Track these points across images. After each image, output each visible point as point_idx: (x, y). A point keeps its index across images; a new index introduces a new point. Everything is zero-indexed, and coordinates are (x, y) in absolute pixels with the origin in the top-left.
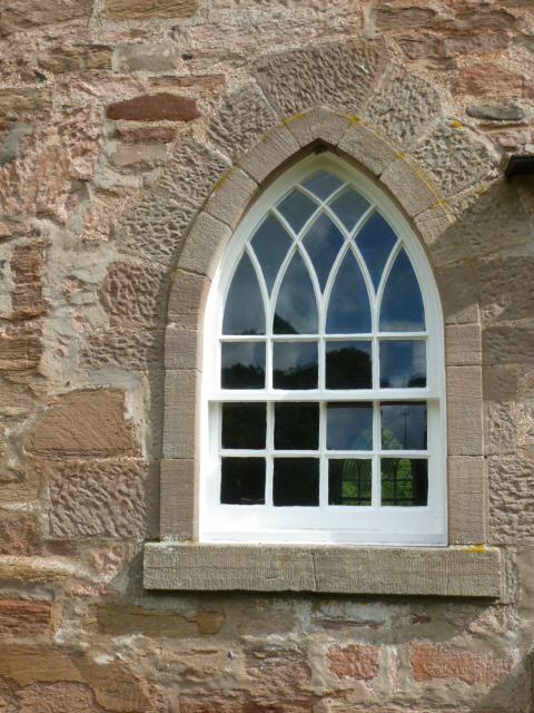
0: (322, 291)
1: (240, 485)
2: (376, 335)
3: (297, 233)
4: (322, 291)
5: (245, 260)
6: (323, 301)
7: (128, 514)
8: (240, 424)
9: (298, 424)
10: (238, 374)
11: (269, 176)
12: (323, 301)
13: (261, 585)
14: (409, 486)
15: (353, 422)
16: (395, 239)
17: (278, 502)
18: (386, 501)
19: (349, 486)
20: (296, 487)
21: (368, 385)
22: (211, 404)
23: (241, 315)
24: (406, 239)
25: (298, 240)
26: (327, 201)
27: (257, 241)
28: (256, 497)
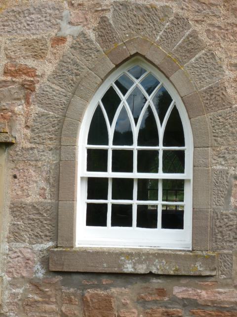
0: (136, 125)
1: (96, 217)
2: (110, 147)
3: (149, 95)
4: (136, 125)
5: (98, 111)
6: (161, 130)
7: (219, 243)
8: (96, 188)
9: (123, 188)
10: (96, 160)
11: (109, 72)
12: (161, 130)
13: (192, 273)
14: (173, 220)
15: (147, 189)
16: (172, 100)
17: (114, 224)
18: (113, 224)
19: (147, 219)
20: (122, 217)
21: (105, 170)
22: (82, 178)
23: (97, 133)
24: (177, 101)
25: (150, 98)
26: (140, 79)
27: (104, 100)
28: (153, 225)
